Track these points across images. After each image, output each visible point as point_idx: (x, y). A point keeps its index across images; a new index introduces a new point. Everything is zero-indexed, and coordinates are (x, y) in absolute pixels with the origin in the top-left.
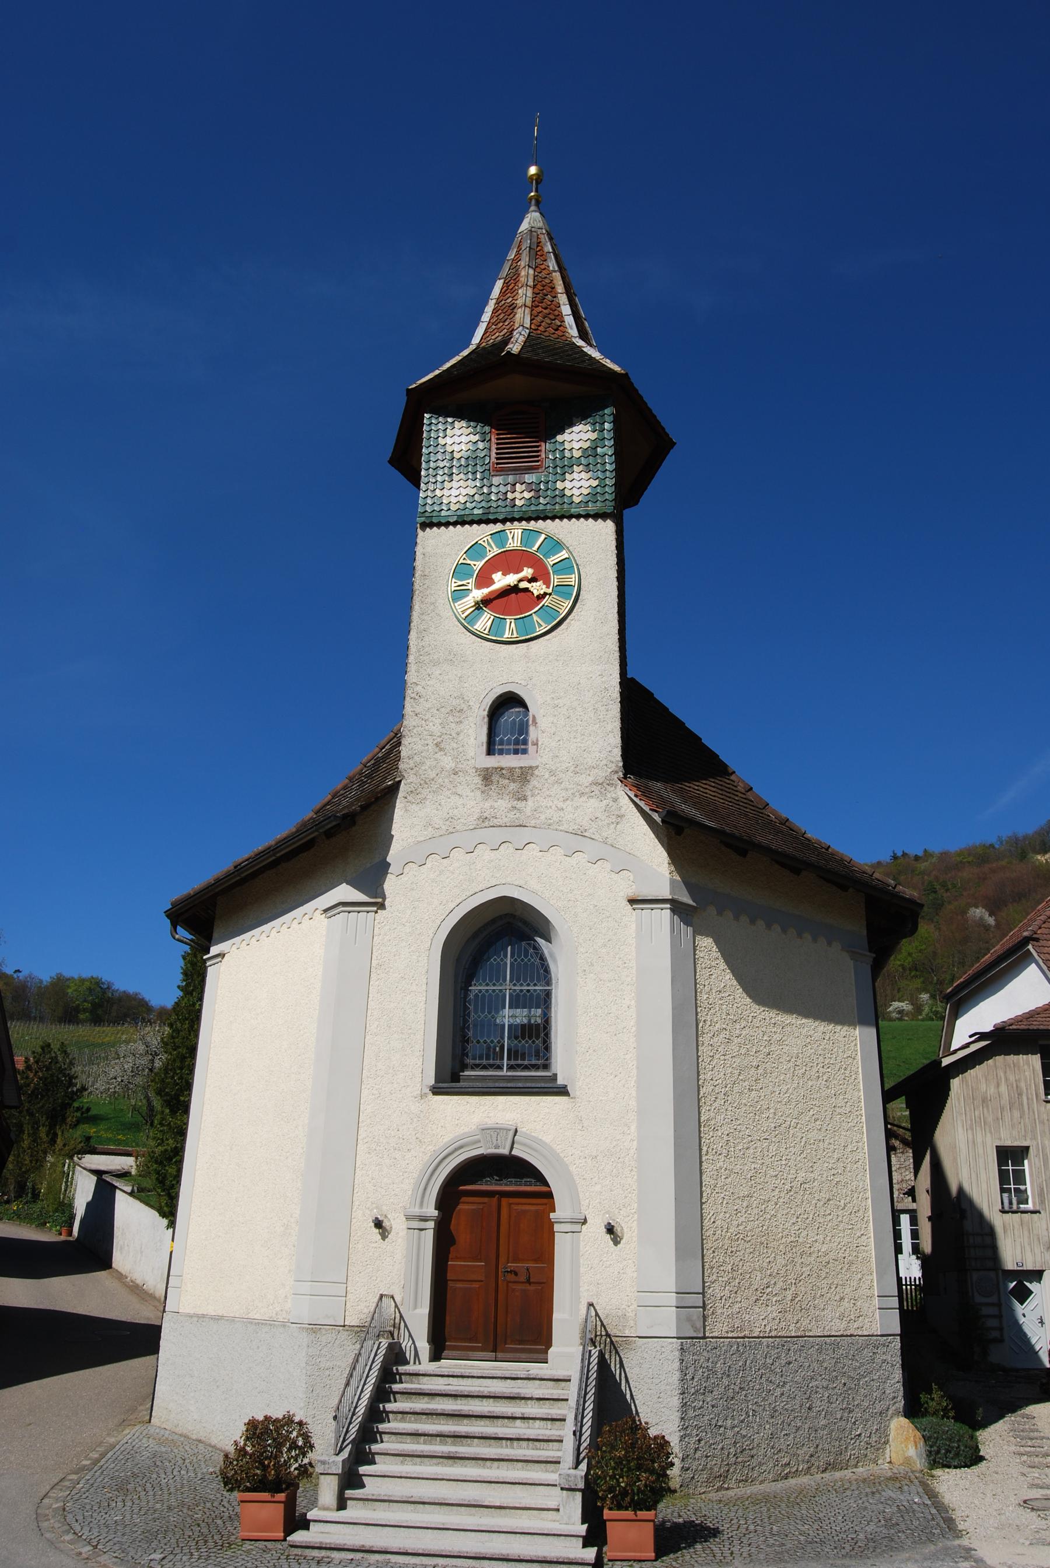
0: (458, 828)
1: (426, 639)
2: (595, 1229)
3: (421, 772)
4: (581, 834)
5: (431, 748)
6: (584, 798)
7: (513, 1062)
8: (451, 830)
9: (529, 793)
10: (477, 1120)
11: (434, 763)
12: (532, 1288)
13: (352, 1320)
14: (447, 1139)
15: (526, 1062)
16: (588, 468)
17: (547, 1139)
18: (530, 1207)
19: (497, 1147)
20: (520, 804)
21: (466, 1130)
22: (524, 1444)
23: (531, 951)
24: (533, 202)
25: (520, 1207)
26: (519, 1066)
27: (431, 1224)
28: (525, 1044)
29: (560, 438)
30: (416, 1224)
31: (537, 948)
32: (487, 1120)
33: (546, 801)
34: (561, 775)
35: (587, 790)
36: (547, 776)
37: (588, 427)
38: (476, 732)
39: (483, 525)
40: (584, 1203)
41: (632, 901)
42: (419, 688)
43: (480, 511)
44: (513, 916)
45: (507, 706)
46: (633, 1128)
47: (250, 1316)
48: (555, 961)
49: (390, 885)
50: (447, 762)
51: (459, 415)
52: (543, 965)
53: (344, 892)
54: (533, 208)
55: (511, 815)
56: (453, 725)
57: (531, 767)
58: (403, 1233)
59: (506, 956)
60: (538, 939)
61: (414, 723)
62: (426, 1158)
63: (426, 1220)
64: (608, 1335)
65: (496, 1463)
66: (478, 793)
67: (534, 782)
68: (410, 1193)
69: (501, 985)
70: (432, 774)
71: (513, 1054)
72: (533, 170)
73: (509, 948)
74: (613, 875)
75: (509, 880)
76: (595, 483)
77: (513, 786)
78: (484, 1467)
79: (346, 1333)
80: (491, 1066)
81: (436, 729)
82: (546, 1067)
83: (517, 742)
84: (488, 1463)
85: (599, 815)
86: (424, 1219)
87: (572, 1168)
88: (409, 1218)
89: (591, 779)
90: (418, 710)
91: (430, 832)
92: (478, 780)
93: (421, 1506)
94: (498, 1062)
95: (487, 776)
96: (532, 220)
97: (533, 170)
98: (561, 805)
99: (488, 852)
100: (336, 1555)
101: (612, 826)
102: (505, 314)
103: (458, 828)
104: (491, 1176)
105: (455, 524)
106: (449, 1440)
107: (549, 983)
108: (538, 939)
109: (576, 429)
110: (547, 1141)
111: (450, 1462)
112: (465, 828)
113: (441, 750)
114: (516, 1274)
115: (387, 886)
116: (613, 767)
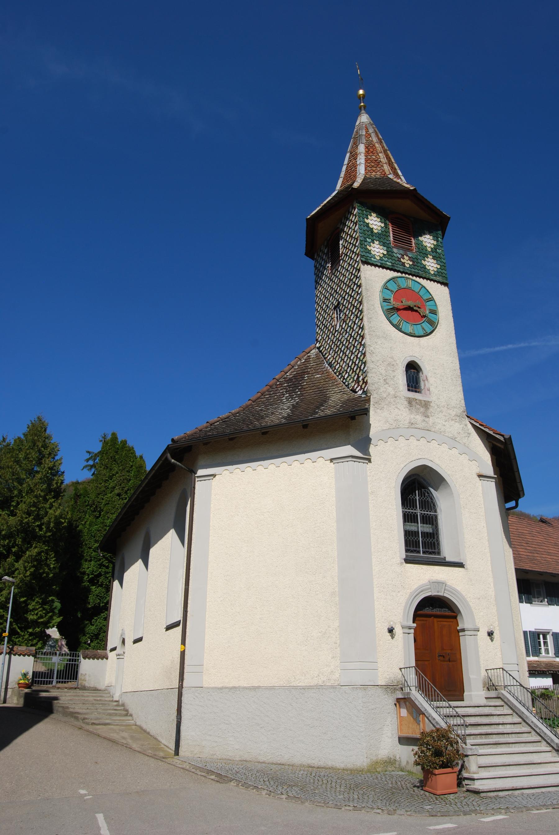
0: (400, 426)
1: (372, 323)
2: (483, 634)
3: (379, 393)
4: (454, 439)
5: (382, 381)
6: (453, 422)
7: (424, 550)
8: (397, 426)
9: (429, 414)
10: (424, 578)
11: (385, 390)
12: (450, 663)
13: (381, 682)
14: (415, 587)
15: (430, 550)
16: (434, 258)
17: (459, 588)
18: (445, 623)
19: (438, 592)
20: (427, 419)
21: (424, 582)
22: (513, 735)
23: (426, 494)
24: (363, 108)
25: (442, 623)
26: (427, 552)
27: (412, 631)
28: (429, 540)
29: (420, 238)
30: (407, 631)
31: (430, 493)
32: (432, 578)
33: (438, 420)
34: (442, 408)
35: (454, 418)
36: (436, 407)
37: (431, 237)
38: (401, 379)
39: (392, 271)
40: (477, 621)
41: (480, 476)
42: (372, 348)
43: (390, 264)
44: (418, 475)
45: (413, 369)
46: (492, 585)
47: (292, 684)
48: (439, 500)
49: (372, 449)
50: (390, 390)
51: (375, 212)
52: (432, 502)
53: (348, 450)
54: (363, 111)
55: (423, 424)
56: (391, 372)
57: (429, 402)
58: (401, 635)
59: (416, 495)
60: (431, 489)
61: (372, 366)
62: (407, 596)
63: (410, 629)
64: (493, 685)
65: (514, 745)
66: (407, 410)
67: (431, 410)
68: (402, 614)
69: (415, 510)
70: (385, 396)
71: (424, 546)
72: (361, 92)
73: (417, 492)
74: (470, 462)
75: (426, 457)
76: (439, 267)
77: (422, 410)
78: (509, 747)
79: (380, 689)
80: (415, 551)
81: (383, 372)
82: (439, 553)
83: (416, 388)
84: (511, 745)
85: (460, 431)
86: (410, 628)
87: (471, 604)
88: (403, 627)
89: (454, 413)
90: (373, 359)
91: (387, 426)
92: (406, 403)
93: (508, 767)
94: (418, 549)
95: (410, 402)
96: (364, 118)
97: (361, 92)
98: (444, 423)
99: (415, 441)
100: (501, 794)
101: (467, 438)
102: (362, 164)
103: (400, 426)
104: (429, 607)
105: (379, 267)
106: (483, 736)
107: (436, 511)
108: (431, 489)
109: (426, 236)
110: (459, 590)
111: (495, 746)
112: (404, 427)
113: (387, 383)
114: (444, 657)
115: (370, 450)
116: (463, 410)
